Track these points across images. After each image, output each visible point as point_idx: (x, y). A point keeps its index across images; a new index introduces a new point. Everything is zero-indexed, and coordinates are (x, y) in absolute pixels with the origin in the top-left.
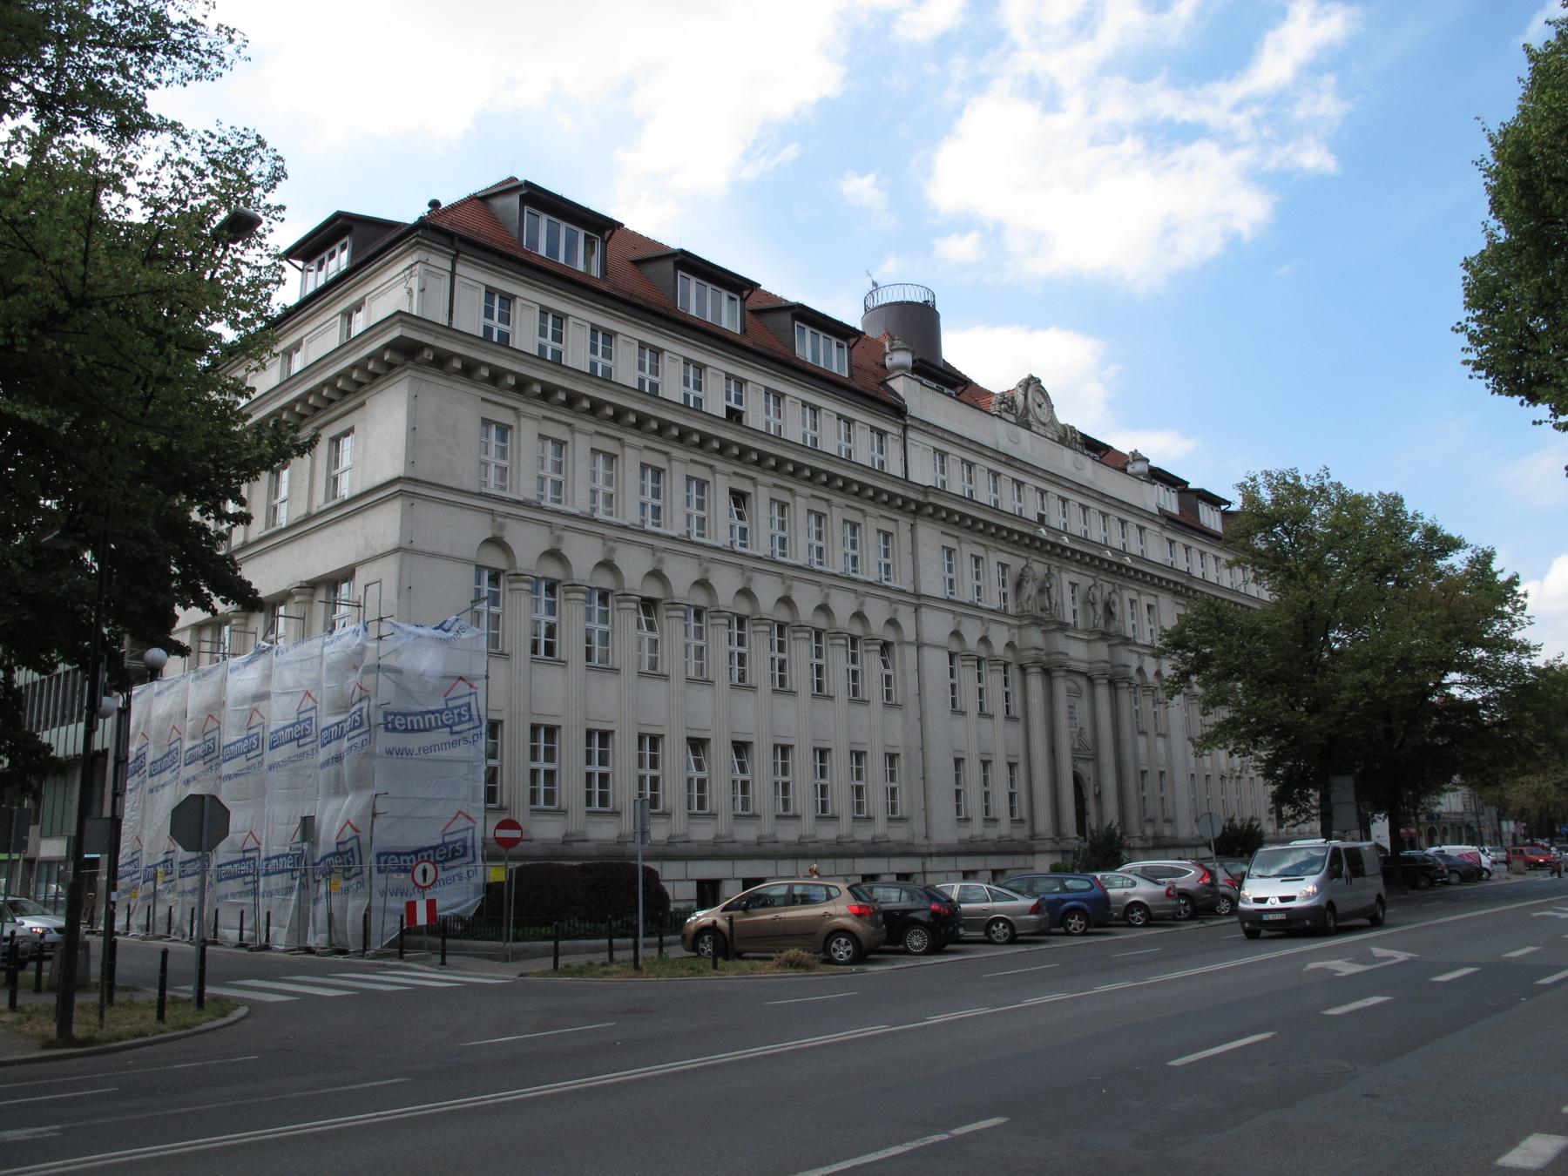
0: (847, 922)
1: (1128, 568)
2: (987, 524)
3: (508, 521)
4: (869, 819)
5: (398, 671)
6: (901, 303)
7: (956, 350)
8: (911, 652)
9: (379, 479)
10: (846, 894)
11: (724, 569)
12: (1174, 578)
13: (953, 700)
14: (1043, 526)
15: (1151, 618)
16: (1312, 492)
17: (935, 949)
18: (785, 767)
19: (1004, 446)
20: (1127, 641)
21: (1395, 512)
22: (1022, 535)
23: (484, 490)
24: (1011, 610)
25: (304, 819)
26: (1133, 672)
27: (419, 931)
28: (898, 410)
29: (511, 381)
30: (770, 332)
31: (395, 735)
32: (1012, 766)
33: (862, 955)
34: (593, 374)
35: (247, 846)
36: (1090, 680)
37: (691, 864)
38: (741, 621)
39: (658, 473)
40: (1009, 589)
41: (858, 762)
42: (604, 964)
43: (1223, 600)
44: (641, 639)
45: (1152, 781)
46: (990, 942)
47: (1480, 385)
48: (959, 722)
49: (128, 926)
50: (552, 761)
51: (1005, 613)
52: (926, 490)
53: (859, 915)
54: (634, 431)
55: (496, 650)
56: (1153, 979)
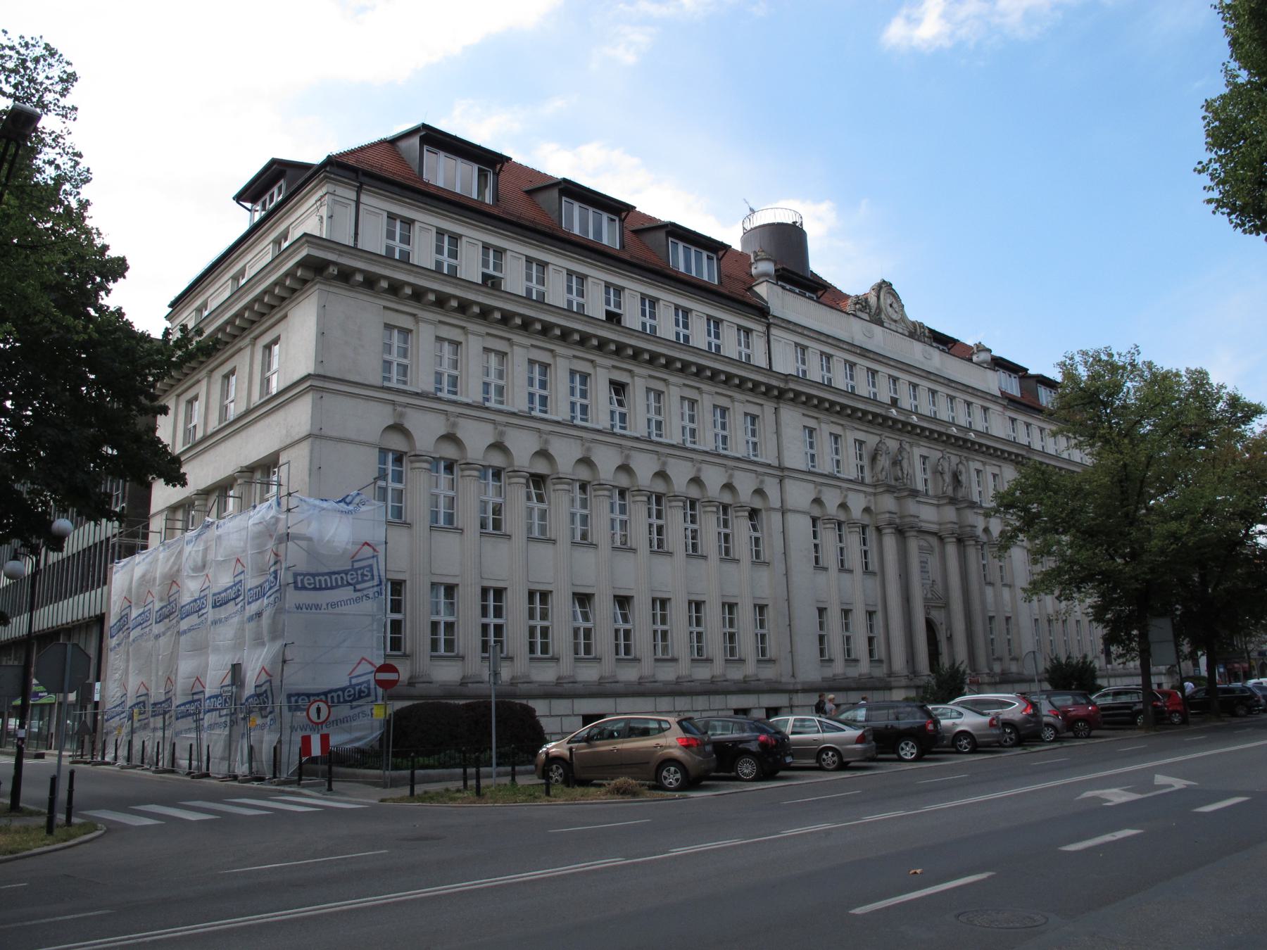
0: (677, 753)
1: (973, 443)
2: (844, 407)
3: (408, 410)
4: (742, 661)
5: (310, 539)
6: (773, 224)
7: (820, 264)
8: (776, 517)
9: (296, 377)
10: (676, 727)
11: (603, 448)
12: (1015, 451)
13: (817, 559)
14: (893, 404)
15: (988, 481)
16: (1124, 368)
17: (766, 774)
18: (731, 621)
19: (859, 339)
20: (972, 505)
21: (1202, 385)
22: (875, 415)
23: (386, 384)
24: (868, 480)
25: (234, 666)
26: (979, 531)
27: (314, 760)
28: (761, 311)
29: (498, 315)
30: (650, 250)
31: (304, 592)
32: (870, 614)
33: (691, 782)
34: (528, 297)
35: (195, 690)
36: (941, 539)
37: (576, 701)
38: (693, 503)
39: (724, 411)
40: (866, 462)
41: (761, 614)
42: (458, 791)
43: (1048, 465)
44: (531, 510)
45: (999, 625)
46: (821, 768)
47: (1222, 222)
48: (821, 578)
49: (116, 758)
50: (399, 612)
51: (862, 483)
52: (787, 377)
53: (687, 747)
54: (522, 332)
55: (398, 518)
56: (868, 819)
